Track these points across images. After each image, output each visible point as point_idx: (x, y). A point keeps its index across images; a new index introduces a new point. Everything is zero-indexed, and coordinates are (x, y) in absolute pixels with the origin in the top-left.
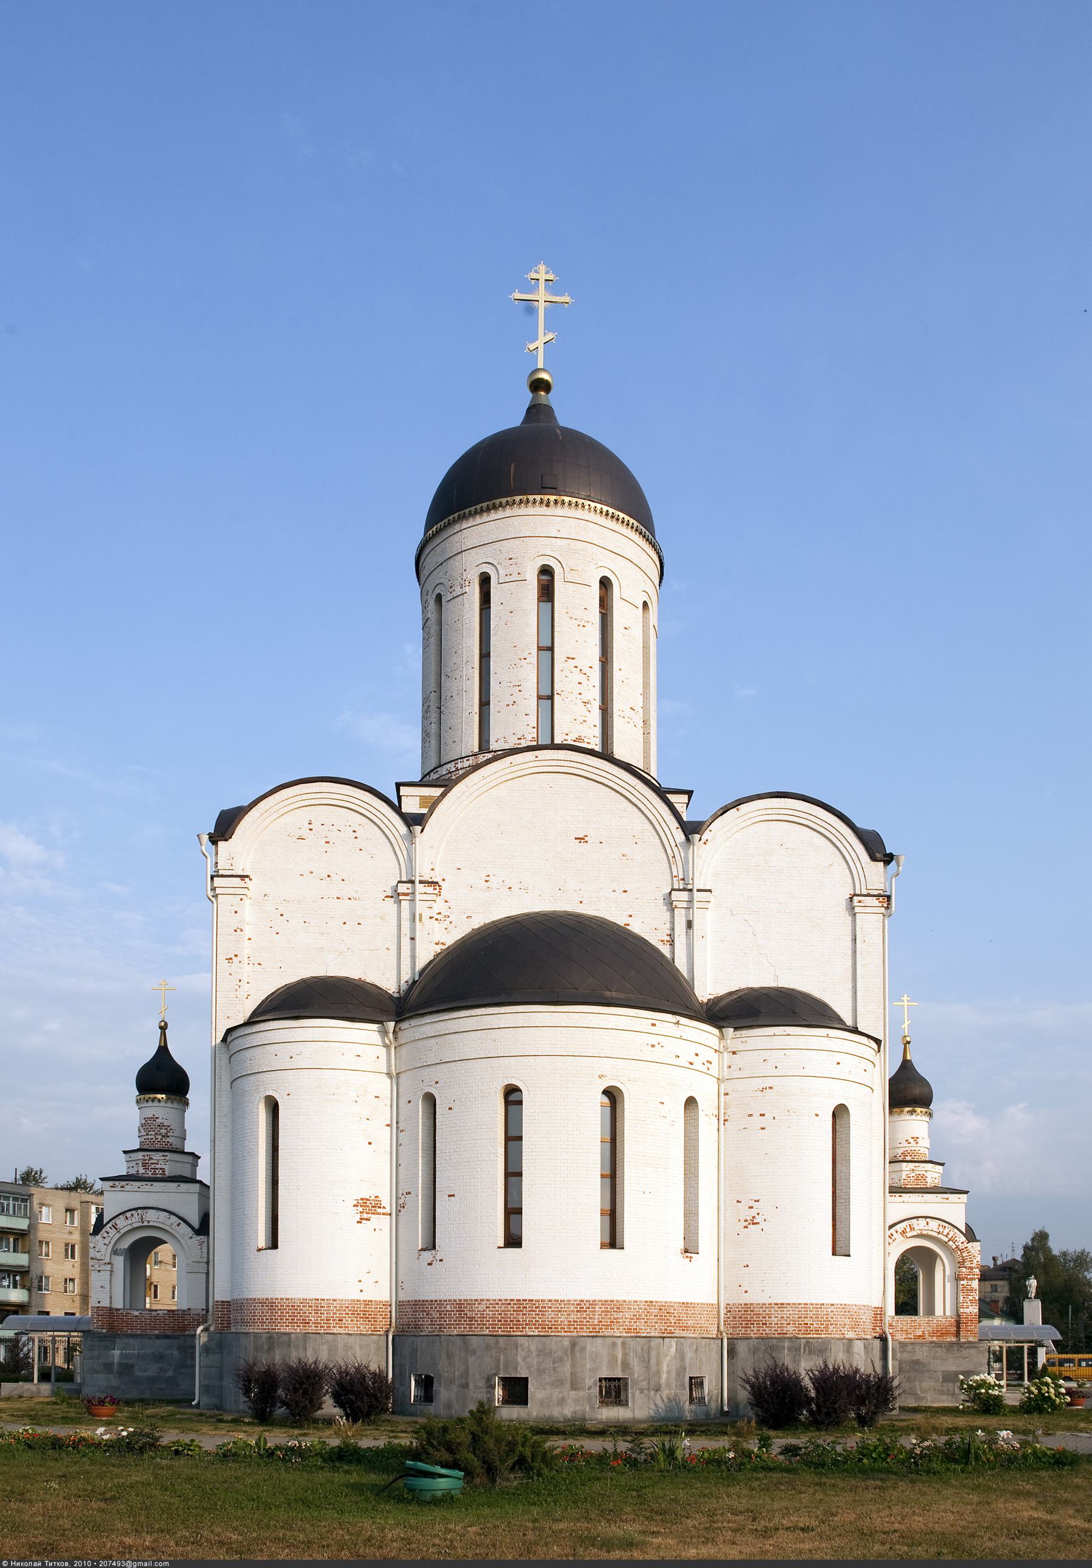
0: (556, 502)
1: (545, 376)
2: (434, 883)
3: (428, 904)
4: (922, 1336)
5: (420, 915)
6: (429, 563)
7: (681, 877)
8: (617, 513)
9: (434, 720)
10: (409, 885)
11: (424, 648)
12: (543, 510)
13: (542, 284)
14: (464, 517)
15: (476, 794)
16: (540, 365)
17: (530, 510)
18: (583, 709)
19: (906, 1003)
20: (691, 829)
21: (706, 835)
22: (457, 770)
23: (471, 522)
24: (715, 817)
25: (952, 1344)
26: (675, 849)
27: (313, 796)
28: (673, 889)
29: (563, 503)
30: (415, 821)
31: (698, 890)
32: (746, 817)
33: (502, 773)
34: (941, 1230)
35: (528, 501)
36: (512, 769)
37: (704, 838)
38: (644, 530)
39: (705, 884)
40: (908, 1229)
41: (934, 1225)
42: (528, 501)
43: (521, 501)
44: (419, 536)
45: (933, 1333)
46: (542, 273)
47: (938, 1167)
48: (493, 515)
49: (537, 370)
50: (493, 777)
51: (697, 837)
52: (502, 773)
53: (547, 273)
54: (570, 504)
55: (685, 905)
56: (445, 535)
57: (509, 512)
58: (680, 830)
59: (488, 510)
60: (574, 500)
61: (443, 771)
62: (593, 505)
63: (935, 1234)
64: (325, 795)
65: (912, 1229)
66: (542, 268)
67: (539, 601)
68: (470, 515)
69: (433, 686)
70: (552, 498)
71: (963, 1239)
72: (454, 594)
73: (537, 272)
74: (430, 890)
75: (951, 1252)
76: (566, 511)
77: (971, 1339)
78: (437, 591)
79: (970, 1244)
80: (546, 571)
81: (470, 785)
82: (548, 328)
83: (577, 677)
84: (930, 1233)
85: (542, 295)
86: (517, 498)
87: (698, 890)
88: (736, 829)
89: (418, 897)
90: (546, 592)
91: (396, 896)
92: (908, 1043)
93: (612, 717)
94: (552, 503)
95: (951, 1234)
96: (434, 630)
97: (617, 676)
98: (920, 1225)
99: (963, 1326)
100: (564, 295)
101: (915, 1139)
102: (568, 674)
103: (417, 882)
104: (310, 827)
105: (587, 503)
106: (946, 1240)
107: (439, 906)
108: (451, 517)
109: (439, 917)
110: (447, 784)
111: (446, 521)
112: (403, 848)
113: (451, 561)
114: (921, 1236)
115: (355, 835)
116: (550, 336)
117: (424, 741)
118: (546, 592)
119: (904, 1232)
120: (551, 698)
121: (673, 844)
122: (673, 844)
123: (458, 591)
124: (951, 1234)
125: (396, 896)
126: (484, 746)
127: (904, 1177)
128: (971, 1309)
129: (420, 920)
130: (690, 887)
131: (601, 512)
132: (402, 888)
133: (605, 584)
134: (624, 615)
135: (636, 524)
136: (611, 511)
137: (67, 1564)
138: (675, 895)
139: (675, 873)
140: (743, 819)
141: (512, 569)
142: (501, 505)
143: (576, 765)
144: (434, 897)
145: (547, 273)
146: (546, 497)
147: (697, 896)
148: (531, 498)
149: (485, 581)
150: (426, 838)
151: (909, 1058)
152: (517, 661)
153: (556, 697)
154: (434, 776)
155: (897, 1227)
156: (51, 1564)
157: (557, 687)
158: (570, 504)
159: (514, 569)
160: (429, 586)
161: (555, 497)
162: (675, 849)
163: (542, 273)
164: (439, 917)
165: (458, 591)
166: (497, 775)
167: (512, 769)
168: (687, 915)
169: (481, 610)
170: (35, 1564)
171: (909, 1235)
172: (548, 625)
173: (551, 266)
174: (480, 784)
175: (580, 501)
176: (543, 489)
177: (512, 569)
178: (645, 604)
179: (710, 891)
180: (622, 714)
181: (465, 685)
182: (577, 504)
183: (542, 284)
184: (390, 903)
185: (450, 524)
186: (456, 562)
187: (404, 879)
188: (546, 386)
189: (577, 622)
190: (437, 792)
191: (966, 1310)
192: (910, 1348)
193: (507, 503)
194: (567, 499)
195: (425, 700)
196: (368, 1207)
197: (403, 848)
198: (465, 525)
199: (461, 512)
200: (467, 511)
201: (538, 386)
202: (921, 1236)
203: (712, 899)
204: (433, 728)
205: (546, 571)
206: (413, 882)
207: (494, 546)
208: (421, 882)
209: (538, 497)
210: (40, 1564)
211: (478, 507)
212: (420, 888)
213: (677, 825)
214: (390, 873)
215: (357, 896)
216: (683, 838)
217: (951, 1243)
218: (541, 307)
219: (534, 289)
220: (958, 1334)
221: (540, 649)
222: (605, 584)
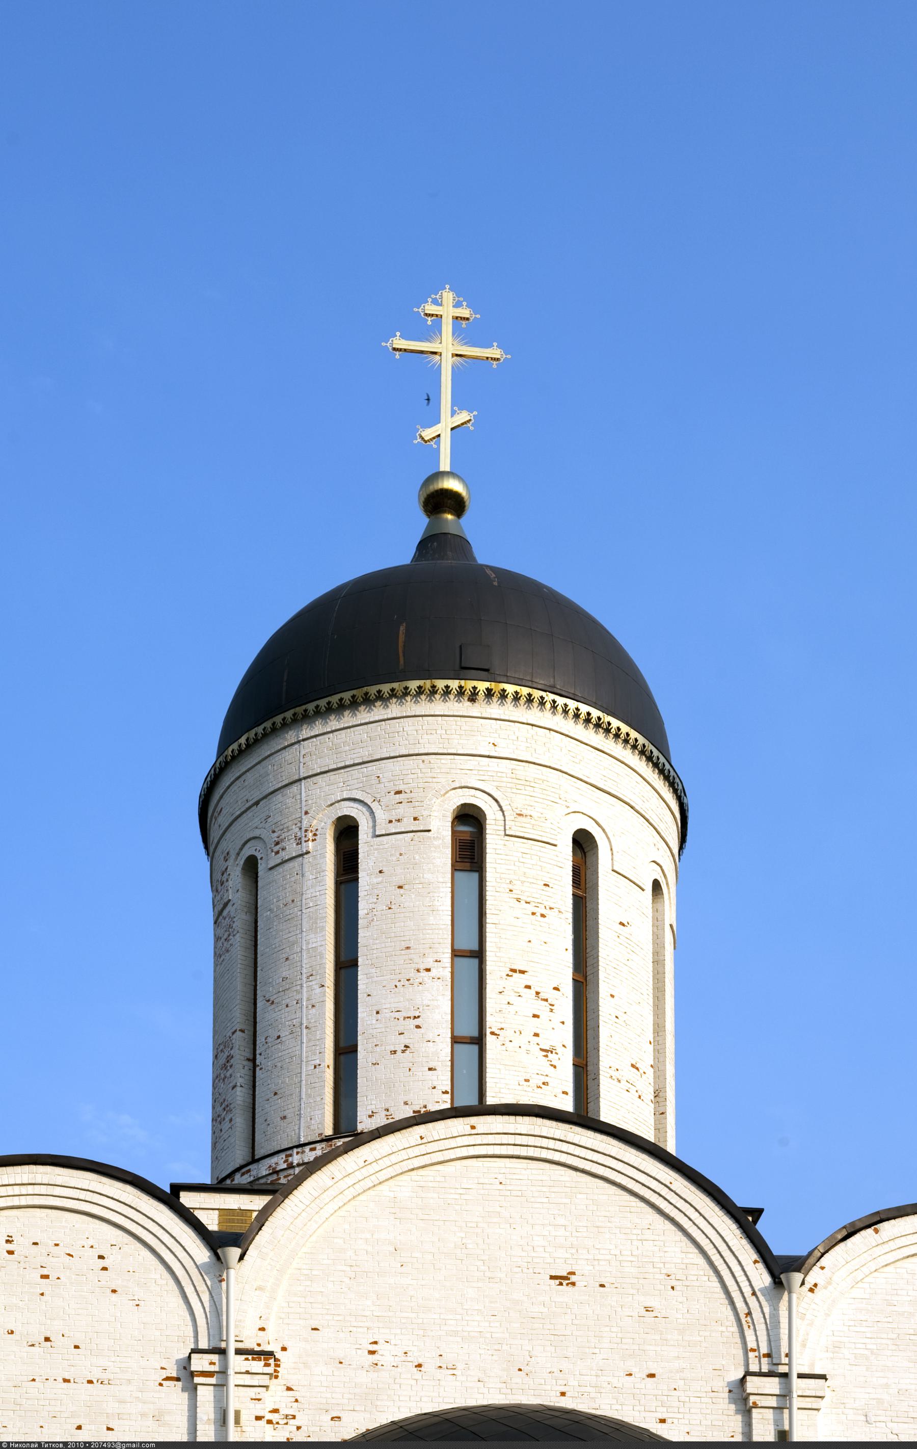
0: (489, 693)
1: (452, 484)
2: (265, 1355)
3: (252, 1392)
5: (237, 1414)
6: (230, 802)
7: (764, 1350)
9: (240, 1081)
10: (215, 1358)
11: (218, 956)
12: (464, 707)
13: (447, 327)
15: (349, 1194)
18: (542, 1063)
20: (782, 1269)
21: (815, 1275)
22: (291, 1166)
24: (832, 1244)
26: (752, 1301)
27: (17, 1190)
28: (748, 1373)
30: (225, 1241)
31: (801, 1376)
32: (892, 1245)
33: (404, 1155)
35: (434, 691)
36: (423, 1149)
37: (811, 1279)
38: (656, 753)
39: (812, 1365)
42: (434, 691)
43: (420, 691)
44: (208, 758)
46: (447, 307)
48: (364, 715)
49: (439, 475)
50: (387, 1162)
51: (797, 1277)
52: (404, 1155)
53: (457, 305)
55: (773, 1402)
56: (265, 750)
57: (394, 709)
58: (761, 1266)
59: (354, 705)
60: (525, 691)
61: (262, 1169)
62: (561, 701)
64: (43, 1190)
66: (448, 296)
67: (455, 869)
69: (238, 1016)
70: (482, 686)
72: (285, 855)
73: (436, 302)
74: (257, 1366)
76: (508, 710)
78: (248, 852)
80: (469, 820)
81: (338, 1176)
82: (458, 404)
83: (530, 1004)
85: (447, 345)
86: (413, 685)
87: (801, 1376)
88: (873, 1266)
89: (233, 1379)
90: (469, 851)
91: (186, 1376)
93: (596, 1078)
94: (481, 695)
96: (240, 920)
97: (607, 1009)
102: (513, 999)
103: (231, 1352)
104: (10, 1247)
105: (549, 697)
107: (275, 1396)
108: (278, 719)
109: (274, 1417)
110: (277, 1190)
111: (268, 724)
112: (202, 1288)
113: (279, 797)
115: (102, 1263)
116: (463, 416)
117: (217, 1119)
118: (469, 851)
120: (479, 1041)
121: (747, 1291)
122: (747, 1291)
123: (292, 849)
125: (186, 1376)
126: (343, 1127)
129: (237, 1422)
130: (783, 1369)
132: (200, 1363)
133: (583, 844)
134: (616, 902)
135: (642, 740)
138: (753, 1384)
139: (751, 1344)
140: (886, 1248)
141: (400, 811)
142: (380, 697)
143: (551, 1144)
144: (265, 1380)
145: (457, 305)
146: (469, 685)
147: (798, 1386)
148: (441, 684)
149: (347, 832)
150: (248, 1272)
152: (412, 974)
153: (490, 1040)
154: (239, 1180)
157: (491, 1022)
160: (231, 843)
161: (487, 685)
162: (752, 1301)
163: (447, 307)
164: (274, 1417)
165: (292, 849)
166: (394, 1159)
167: (423, 1149)
168: (778, 1422)
169: (338, 884)
172: (473, 913)
173: (463, 296)
174: (359, 1175)
175: (537, 694)
176: (463, 671)
177: (400, 811)
178: (656, 885)
179: (823, 1377)
180: (616, 1075)
181: (307, 1016)
183: (447, 327)
184: (176, 1396)
185: (274, 731)
187: (203, 1344)
188: (456, 503)
189: (531, 908)
190: (256, 1203)
193: (393, 694)
194: (510, 689)
195: (221, 1048)
196: (755, 1262)
197: (202, 1288)
198: (305, 732)
199: (300, 710)
200: (311, 707)
201: (440, 502)
203: (828, 1393)
204: (240, 1096)
205: (469, 820)
206: (222, 1352)
207: (364, 769)
208: (239, 1352)
209: (454, 684)
211: (335, 699)
212: (236, 1362)
213: (755, 1256)
214: (171, 1330)
215: (104, 1376)
216: (767, 1279)
219: (432, 328)
221: (456, 954)
222: (583, 844)
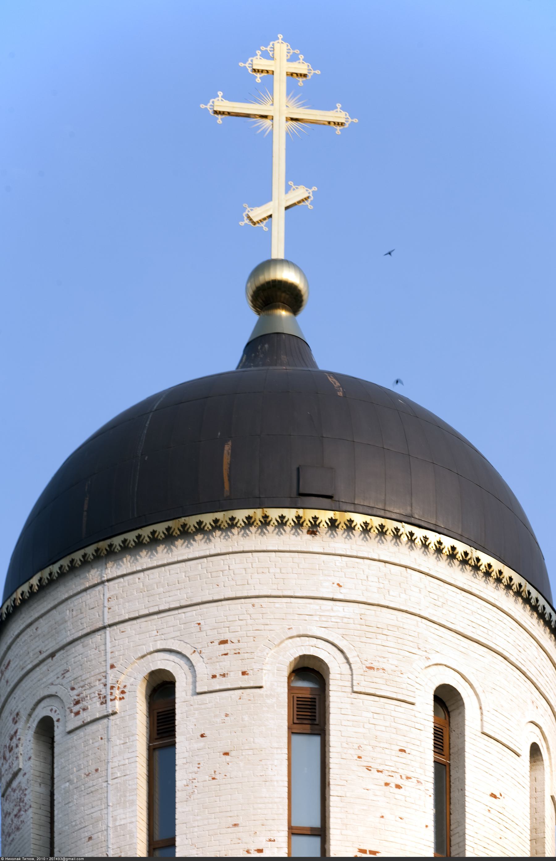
0: (333, 524)
8: (475, 553)
12: (303, 540)
13: (280, 84)
14: (111, 554)
16: (278, 252)
17: (272, 539)
23: (127, 565)
29: (350, 527)
42: (265, 522)
43: (249, 522)
49: (270, 263)
53: (293, 59)
54: (366, 529)
59: (169, 538)
60: (375, 522)
66: (281, 48)
67: (292, 732)
68: (125, 548)
70: (324, 516)
72: (86, 716)
76: (356, 544)
78: (42, 712)
80: (309, 673)
82: (294, 177)
85: (280, 107)
86: (241, 515)
90: (310, 711)
94: (323, 527)
100: (332, 107)
105: (405, 529)
108: (78, 556)
111: (65, 562)
113: (78, 648)
116: (300, 193)
118: (310, 711)
123: (95, 709)
131: (439, 551)
133: (446, 701)
135: (517, 579)
136: (461, 548)
141: (225, 664)
142: (200, 529)
145: (293, 59)
146: (308, 515)
148: (274, 514)
149: (161, 689)
158: (366, 529)
159: (231, 665)
161: (330, 514)
163: (281, 60)
165: (95, 709)
169: (151, 750)
173: (299, 46)
175: (390, 525)
176: (301, 497)
177: (225, 664)
178: (535, 750)
182: (382, 531)
183: (280, 84)
186: (89, 650)
193: (216, 525)
194: (359, 519)
199: (104, 545)
201: (272, 296)
205: (309, 673)
207: (181, 615)
209: (290, 514)
211: (146, 532)
218: (280, 131)
222: (446, 701)
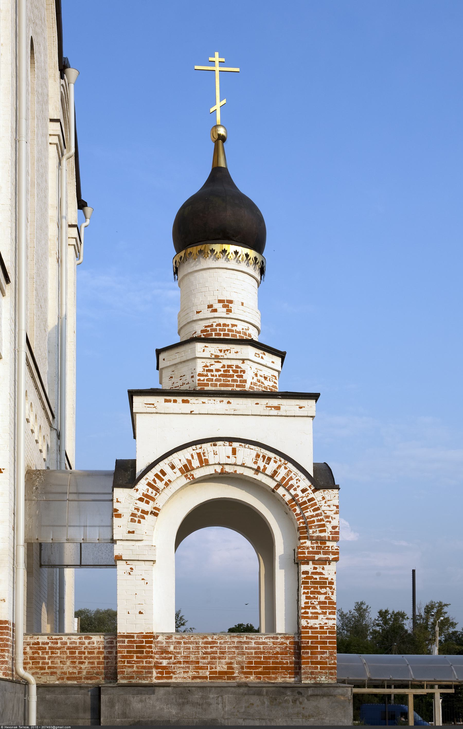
4: (228, 674)
16: (219, 122)
19: (217, 68)
25: (285, 687)
34: (261, 464)
40: (196, 463)
41: (246, 455)
45: (248, 669)
47: (269, 359)
49: (216, 126)
63: (250, 473)
65: (204, 463)
71: (305, 483)
75: (284, 508)
77: (323, 679)
79: (318, 495)
84: (240, 470)
92: (222, 138)
95: (282, 472)
98: (220, 454)
99: (306, 654)
101: (227, 304)
106: (272, 484)
114: (221, 477)
119: (186, 469)
124: (282, 472)
127: (199, 369)
128: (321, 620)
137: (28, 727)
151: (222, 165)
155: (174, 458)
156: (21, 727)
169: (31, 50)
170: (15, 727)
171: (198, 474)
191: (312, 622)
192: (196, 696)
202: (221, 477)
210: (17, 727)
217: (281, 491)
220: (297, 670)
